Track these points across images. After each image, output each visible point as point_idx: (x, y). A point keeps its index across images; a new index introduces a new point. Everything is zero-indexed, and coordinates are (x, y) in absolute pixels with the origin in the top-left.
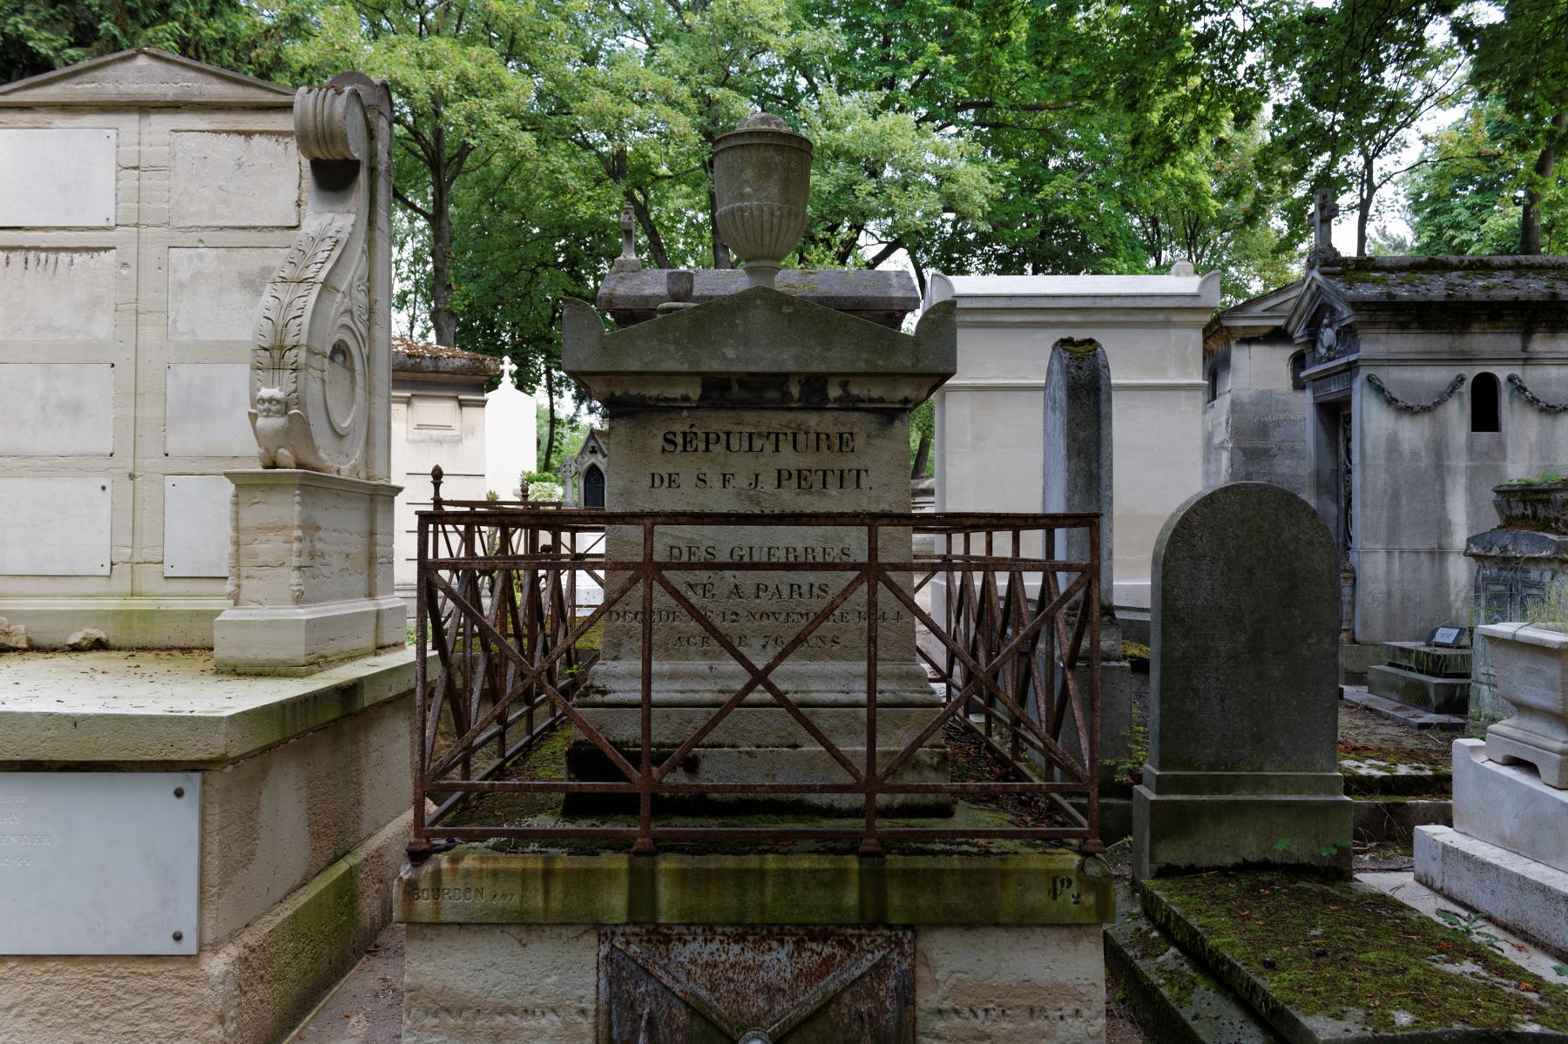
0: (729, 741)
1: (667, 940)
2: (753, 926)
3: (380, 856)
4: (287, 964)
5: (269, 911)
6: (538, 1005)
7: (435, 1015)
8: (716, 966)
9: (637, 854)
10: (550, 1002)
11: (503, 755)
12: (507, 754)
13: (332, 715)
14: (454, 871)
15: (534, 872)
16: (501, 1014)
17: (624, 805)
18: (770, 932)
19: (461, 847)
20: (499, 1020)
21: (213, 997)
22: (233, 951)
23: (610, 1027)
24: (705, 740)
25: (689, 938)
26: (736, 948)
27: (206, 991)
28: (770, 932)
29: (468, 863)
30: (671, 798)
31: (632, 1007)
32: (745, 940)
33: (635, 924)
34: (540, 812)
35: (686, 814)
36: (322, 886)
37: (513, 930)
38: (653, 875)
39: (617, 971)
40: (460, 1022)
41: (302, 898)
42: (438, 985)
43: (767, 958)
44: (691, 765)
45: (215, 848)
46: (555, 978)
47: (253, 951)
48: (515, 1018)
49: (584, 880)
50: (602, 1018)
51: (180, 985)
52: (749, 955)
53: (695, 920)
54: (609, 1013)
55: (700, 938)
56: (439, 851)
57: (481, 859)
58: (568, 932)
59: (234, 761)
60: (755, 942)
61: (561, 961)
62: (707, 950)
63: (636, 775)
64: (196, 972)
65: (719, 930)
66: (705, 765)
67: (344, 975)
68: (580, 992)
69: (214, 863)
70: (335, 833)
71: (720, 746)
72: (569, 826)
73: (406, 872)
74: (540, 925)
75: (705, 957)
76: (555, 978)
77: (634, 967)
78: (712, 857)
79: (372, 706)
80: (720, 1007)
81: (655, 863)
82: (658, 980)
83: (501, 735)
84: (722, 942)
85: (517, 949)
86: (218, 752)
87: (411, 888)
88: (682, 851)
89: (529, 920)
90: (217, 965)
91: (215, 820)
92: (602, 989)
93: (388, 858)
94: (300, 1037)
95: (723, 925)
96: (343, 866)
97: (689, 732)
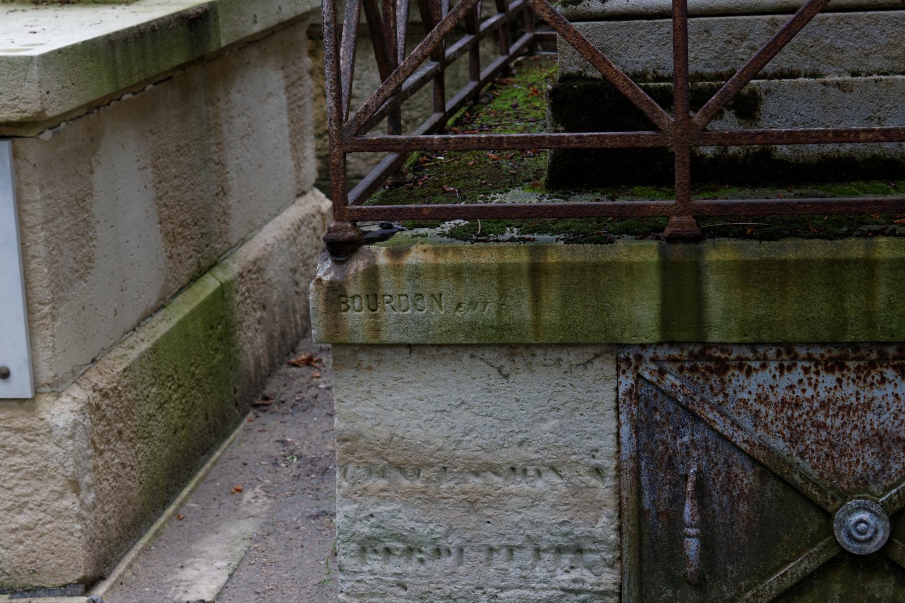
0: (807, 66)
1: (722, 367)
2: (855, 346)
3: (260, 270)
4: (151, 417)
5: (119, 343)
6: (530, 462)
7: (383, 474)
8: (798, 405)
9: (671, 239)
10: (549, 457)
11: (442, 109)
12: (448, 106)
13: (178, 60)
14: (397, 269)
15: (517, 268)
16: (476, 474)
17: (651, 168)
18: (883, 356)
19: (403, 236)
20: (475, 482)
21: (63, 456)
22: (80, 394)
23: (639, 493)
24: (768, 68)
25: (756, 365)
26: (829, 380)
27: (50, 448)
28: (883, 356)
29: (416, 257)
30: (717, 158)
31: (671, 465)
32: (842, 367)
33: (672, 344)
34: (512, 185)
35: (740, 183)
36: (186, 310)
37: (489, 355)
38: (698, 270)
39: (646, 413)
40: (419, 484)
41: (162, 326)
42: (383, 433)
43: (878, 393)
44: (747, 107)
45: (40, 250)
46: (554, 423)
47: (105, 396)
48: (497, 479)
49: (593, 280)
50: (627, 479)
51: (13, 440)
52: (849, 389)
53: (765, 338)
54: (637, 474)
55: (773, 365)
56: (372, 241)
57: (436, 251)
58: (571, 357)
59: (53, 123)
60: (858, 369)
61: (561, 399)
62: (784, 382)
63: (667, 119)
64: (33, 422)
65: (802, 352)
66: (769, 106)
67: (226, 436)
68: (593, 443)
69: (41, 271)
70: (197, 235)
71: (792, 75)
72: (559, 202)
73: (325, 270)
74: (528, 346)
75: (781, 392)
76: (554, 423)
77: (671, 407)
78: (789, 242)
79: (230, 47)
80: (806, 465)
81: (700, 253)
82: (709, 425)
83: (438, 77)
84: (806, 370)
85: (496, 380)
86: (31, 109)
87: (335, 294)
88: (741, 235)
89: (511, 340)
90: (62, 412)
91: (37, 209)
92: (624, 439)
93: (270, 274)
94: (177, 516)
95: (808, 344)
96: (210, 284)
97: (743, 55)
